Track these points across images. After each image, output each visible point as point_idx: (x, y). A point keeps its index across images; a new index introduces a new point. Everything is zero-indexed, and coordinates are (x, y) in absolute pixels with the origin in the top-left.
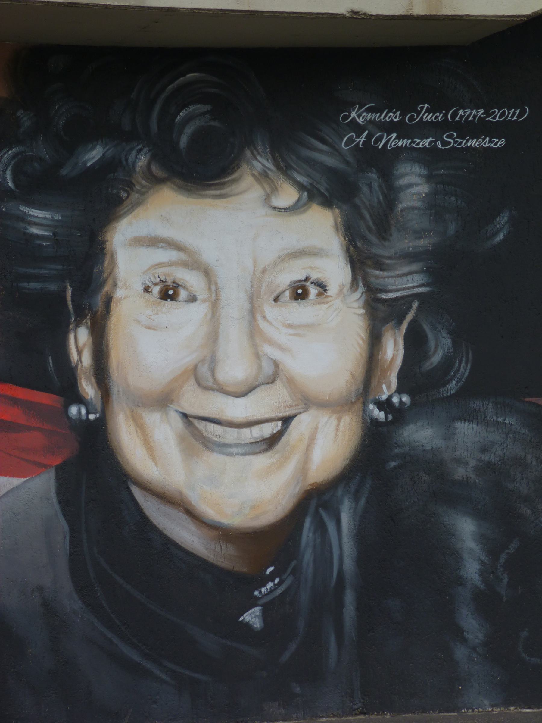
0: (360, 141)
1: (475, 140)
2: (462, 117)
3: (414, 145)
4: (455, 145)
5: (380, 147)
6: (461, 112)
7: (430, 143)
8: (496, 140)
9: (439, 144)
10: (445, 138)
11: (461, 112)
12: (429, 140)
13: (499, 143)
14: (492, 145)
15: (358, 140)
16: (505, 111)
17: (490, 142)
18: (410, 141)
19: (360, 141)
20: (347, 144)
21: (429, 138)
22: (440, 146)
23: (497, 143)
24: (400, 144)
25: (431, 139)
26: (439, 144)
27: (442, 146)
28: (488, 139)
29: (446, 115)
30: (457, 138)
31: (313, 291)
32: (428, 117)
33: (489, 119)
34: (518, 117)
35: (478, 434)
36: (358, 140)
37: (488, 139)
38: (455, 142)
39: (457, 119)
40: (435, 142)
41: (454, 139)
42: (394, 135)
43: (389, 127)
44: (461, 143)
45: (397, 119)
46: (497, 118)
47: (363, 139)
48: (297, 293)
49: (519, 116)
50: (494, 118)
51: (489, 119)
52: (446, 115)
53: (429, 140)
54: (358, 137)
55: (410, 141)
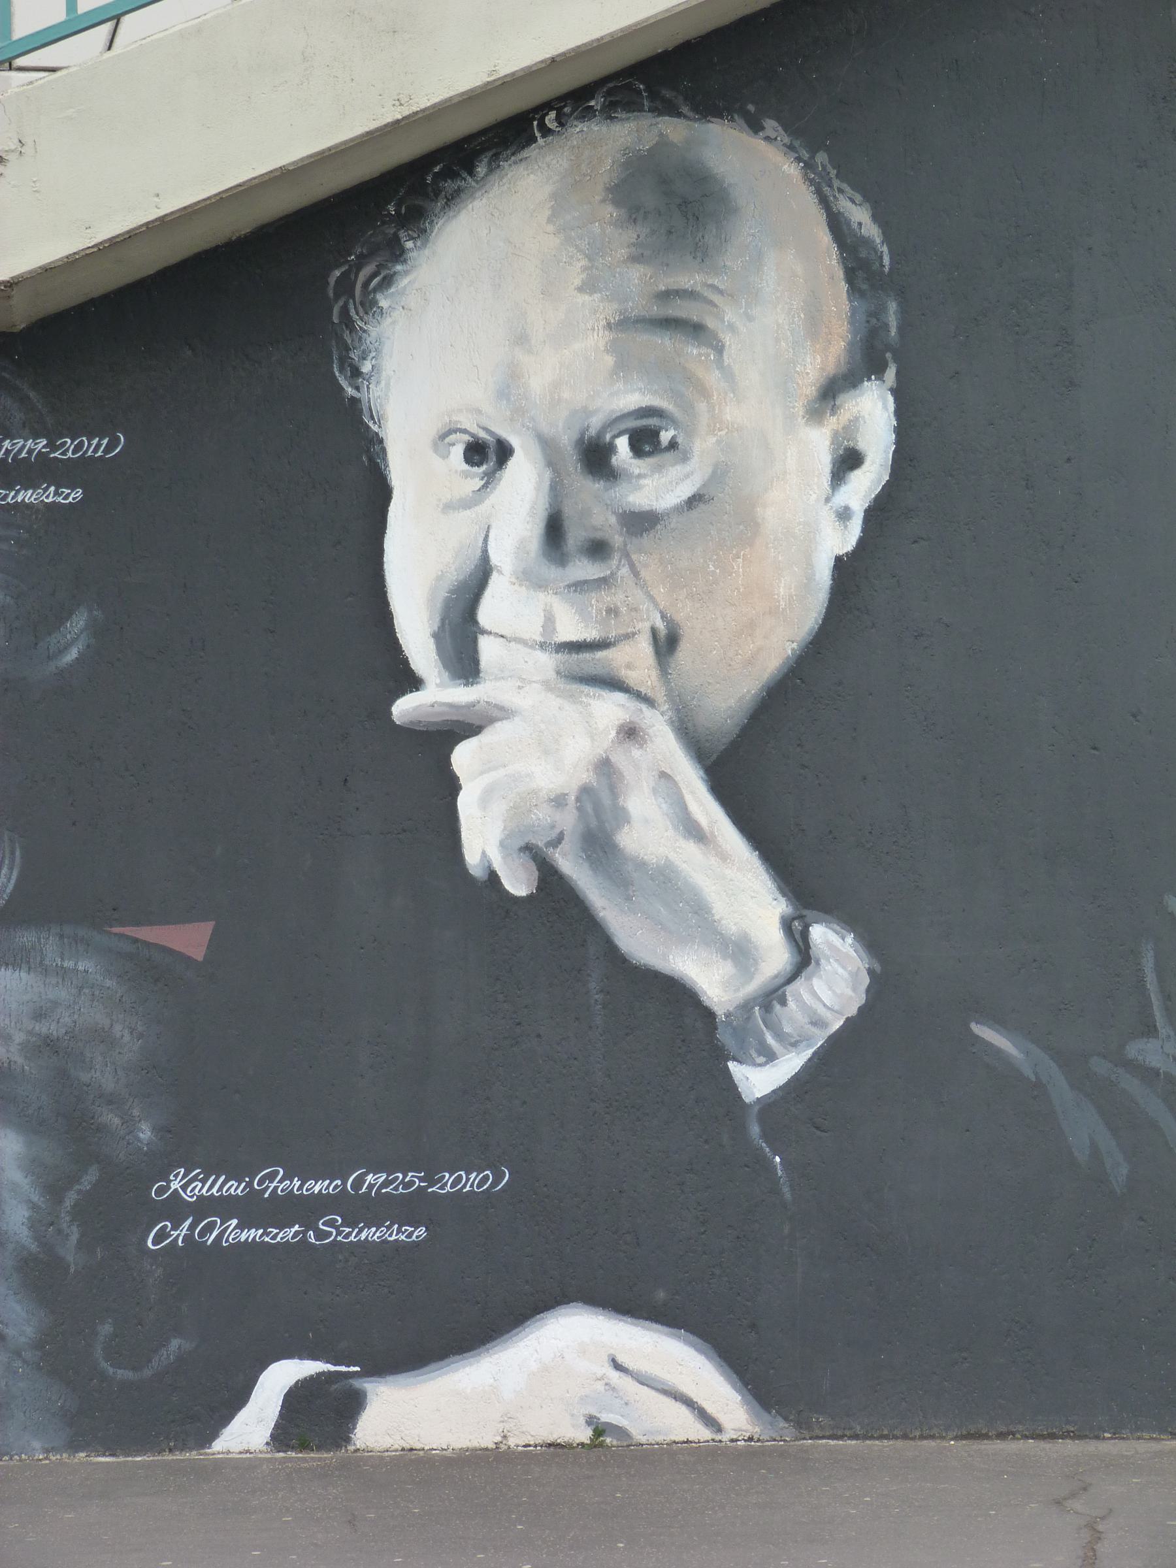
0: (179, 1235)
1: (374, 1229)
2: (371, 1186)
3: (267, 1239)
4: (339, 1238)
5: (209, 1242)
6: (370, 1178)
7: (296, 1234)
8: (276, 1231)
11: (370, 1178)
12: (293, 1230)
13: (72, 495)
14: (60, 499)
15: (176, 1233)
16: (154, 1244)
17: (56, 493)
18: (261, 1231)
21: (293, 1226)
23: (411, 1233)
24: (243, 1238)
25: (296, 1228)
28: (52, 489)
29: (250, 1185)
30: (342, 1225)
34: (106, 451)
35: (635, 659)
36: (176, 1233)
37: (52, 489)
38: (339, 1233)
40: (304, 1233)
42: (234, 1222)
43: (223, 1207)
47: (184, 1231)
49: (496, 1182)
52: (344, 1183)
53: (293, 1230)
54: (175, 1228)
55: (261, 1231)
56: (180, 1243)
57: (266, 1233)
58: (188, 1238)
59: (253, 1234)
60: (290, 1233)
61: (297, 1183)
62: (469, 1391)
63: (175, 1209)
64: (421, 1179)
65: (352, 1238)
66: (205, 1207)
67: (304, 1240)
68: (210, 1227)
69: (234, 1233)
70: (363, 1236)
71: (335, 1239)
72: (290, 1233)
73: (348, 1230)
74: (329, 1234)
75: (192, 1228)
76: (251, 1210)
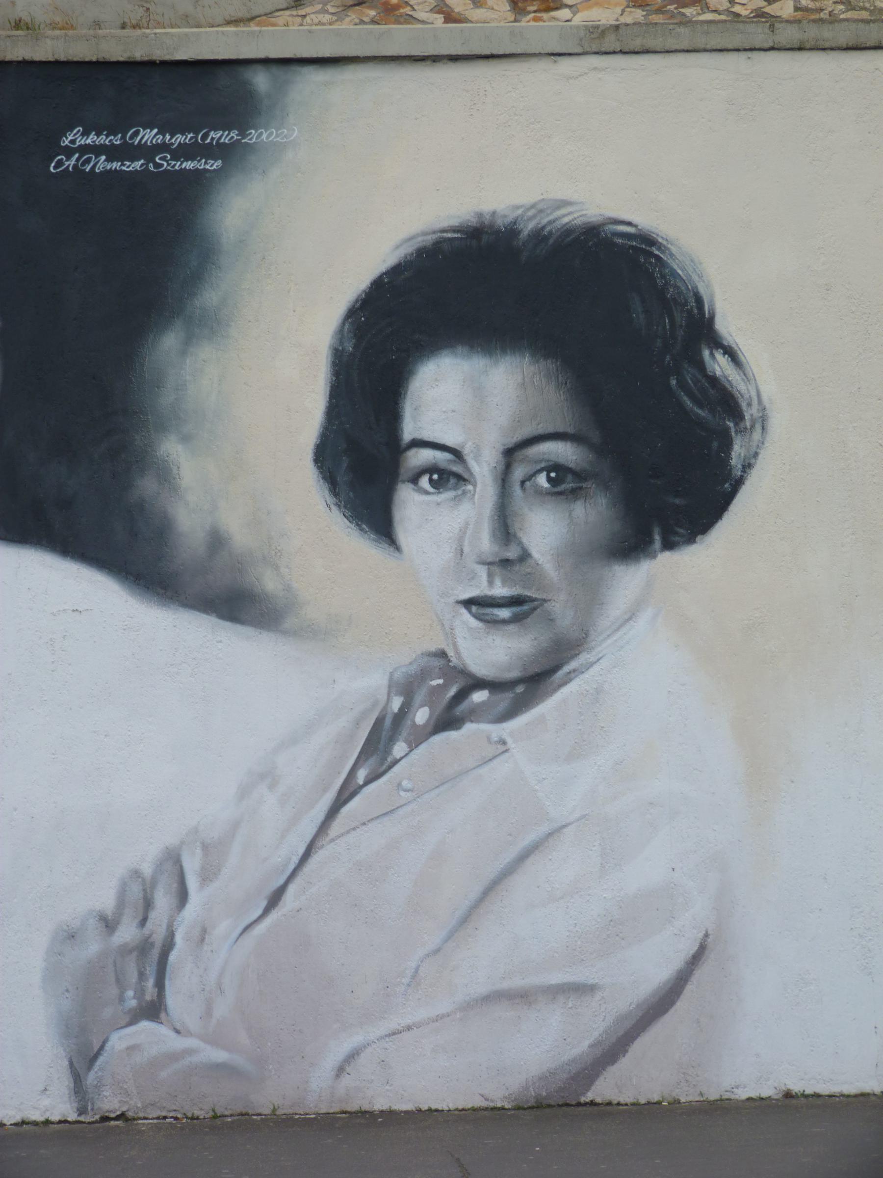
5: (87, 170)
6: (212, 134)
7: (142, 165)
9: (151, 167)
10: (59, 157)
11: (212, 134)
12: (140, 163)
15: (67, 163)
17: (206, 163)
18: (119, 164)
19: (69, 165)
20: (55, 168)
22: (152, 169)
25: (142, 161)
26: (151, 167)
27: (154, 168)
28: (203, 161)
29: (123, 137)
30: (171, 159)
31: (492, 652)
32: (81, 141)
33: (246, 140)
37: (203, 161)
38: (169, 165)
39: (208, 141)
40: (147, 164)
41: (167, 161)
42: (103, 158)
43: (97, 150)
44: (175, 165)
45: (118, 142)
46: (254, 140)
47: (73, 163)
48: (440, 478)
50: (250, 139)
51: (246, 140)
53: (140, 163)
54: (68, 159)
55: (119, 164)
56: (70, 169)
57: (123, 165)
58: (75, 166)
59: (116, 165)
60: (138, 165)
61: (168, 137)
62: (544, 1094)
63: (68, 152)
64: (237, 135)
65: (177, 167)
66: (84, 149)
67: (147, 168)
68: (88, 161)
69: (102, 164)
70: (183, 166)
71: (198, 135)
72: (138, 165)
73: (174, 163)
74: (162, 165)
75: (78, 160)
76: (112, 153)
